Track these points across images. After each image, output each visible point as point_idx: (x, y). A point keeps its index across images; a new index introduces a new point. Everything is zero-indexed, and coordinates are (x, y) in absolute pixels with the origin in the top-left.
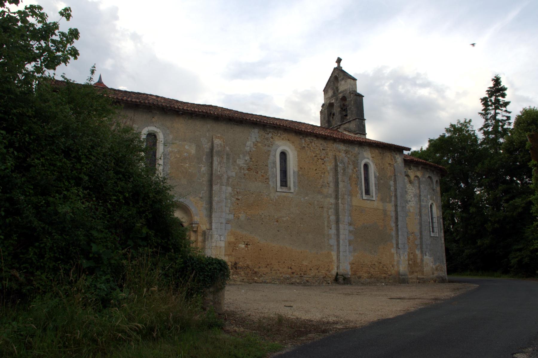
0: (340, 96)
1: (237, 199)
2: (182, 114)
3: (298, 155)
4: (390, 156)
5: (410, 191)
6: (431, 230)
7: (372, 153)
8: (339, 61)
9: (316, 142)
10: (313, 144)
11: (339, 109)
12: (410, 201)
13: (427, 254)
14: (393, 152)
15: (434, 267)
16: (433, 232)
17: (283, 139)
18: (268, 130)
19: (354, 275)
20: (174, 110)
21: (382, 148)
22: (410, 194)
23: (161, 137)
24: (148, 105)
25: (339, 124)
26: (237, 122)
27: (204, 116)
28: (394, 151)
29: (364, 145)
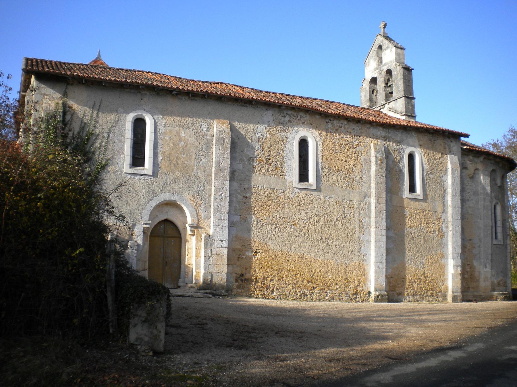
0: (385, 68)
1: (244, 197)
2: (177, 94)
3: (72, 85)
4: (443, 144)
5: (468, 187)
6: (494, 236)
7: (419, 140)
8: (99, 54)
9: (346, 127)
10: (343, 128)
11: (383, 85)
12: (468, 200)
13: (487, 265)
14: (447, 139)
15: (496, 281)
16: (496, 238)
17: (303, 123)
18: (285, 112)
19: (392, 291)
20: (168, 90)
21: (432, 133)
22: (468, 191)
23: (149, 120)
24: (136, 84)
25: (383, 103)
26: (245, 103)
27: (204, 95)
28: (449, 138)
29: (410, 130)
